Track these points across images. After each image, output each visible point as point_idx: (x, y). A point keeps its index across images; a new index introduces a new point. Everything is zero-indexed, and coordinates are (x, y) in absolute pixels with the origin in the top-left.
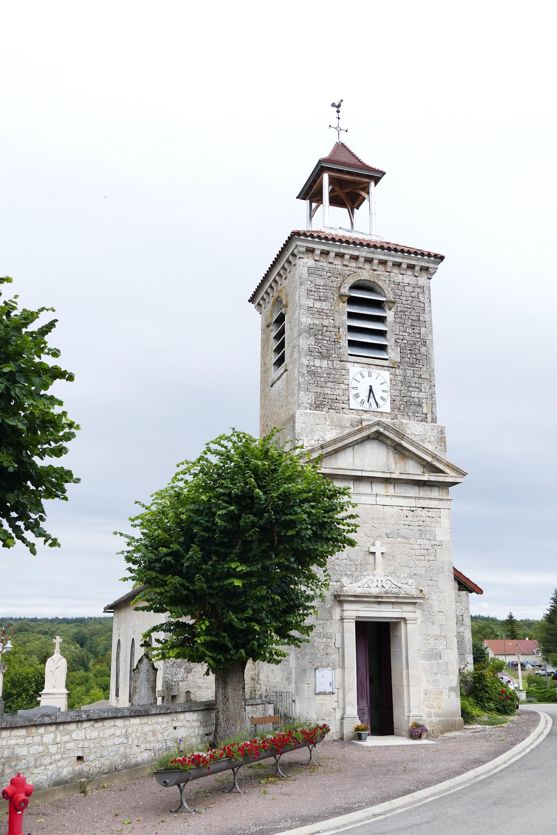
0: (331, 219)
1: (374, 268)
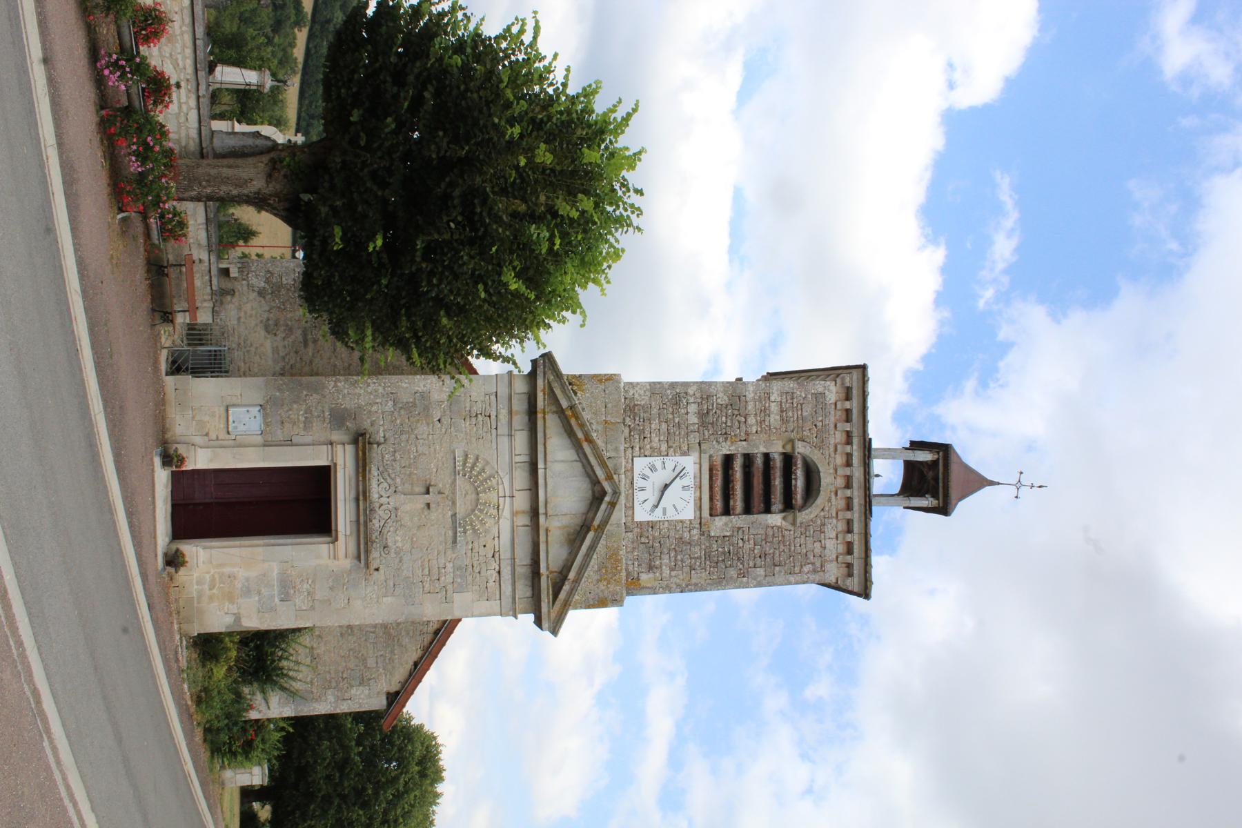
1: (839, 492)
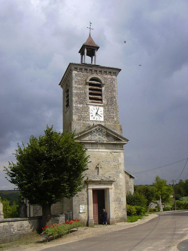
0: (88, 60)
1: (88, 72)
